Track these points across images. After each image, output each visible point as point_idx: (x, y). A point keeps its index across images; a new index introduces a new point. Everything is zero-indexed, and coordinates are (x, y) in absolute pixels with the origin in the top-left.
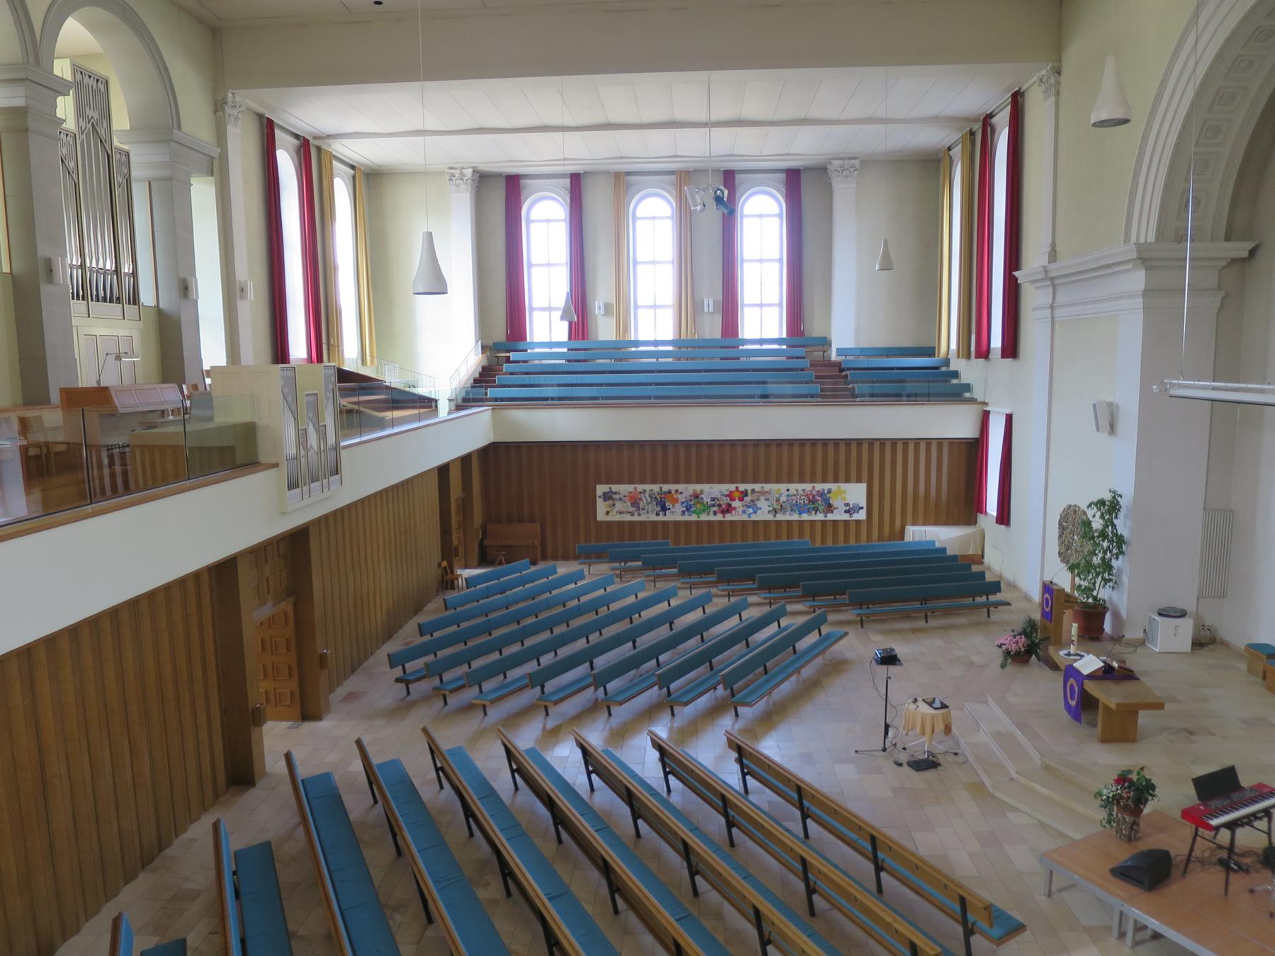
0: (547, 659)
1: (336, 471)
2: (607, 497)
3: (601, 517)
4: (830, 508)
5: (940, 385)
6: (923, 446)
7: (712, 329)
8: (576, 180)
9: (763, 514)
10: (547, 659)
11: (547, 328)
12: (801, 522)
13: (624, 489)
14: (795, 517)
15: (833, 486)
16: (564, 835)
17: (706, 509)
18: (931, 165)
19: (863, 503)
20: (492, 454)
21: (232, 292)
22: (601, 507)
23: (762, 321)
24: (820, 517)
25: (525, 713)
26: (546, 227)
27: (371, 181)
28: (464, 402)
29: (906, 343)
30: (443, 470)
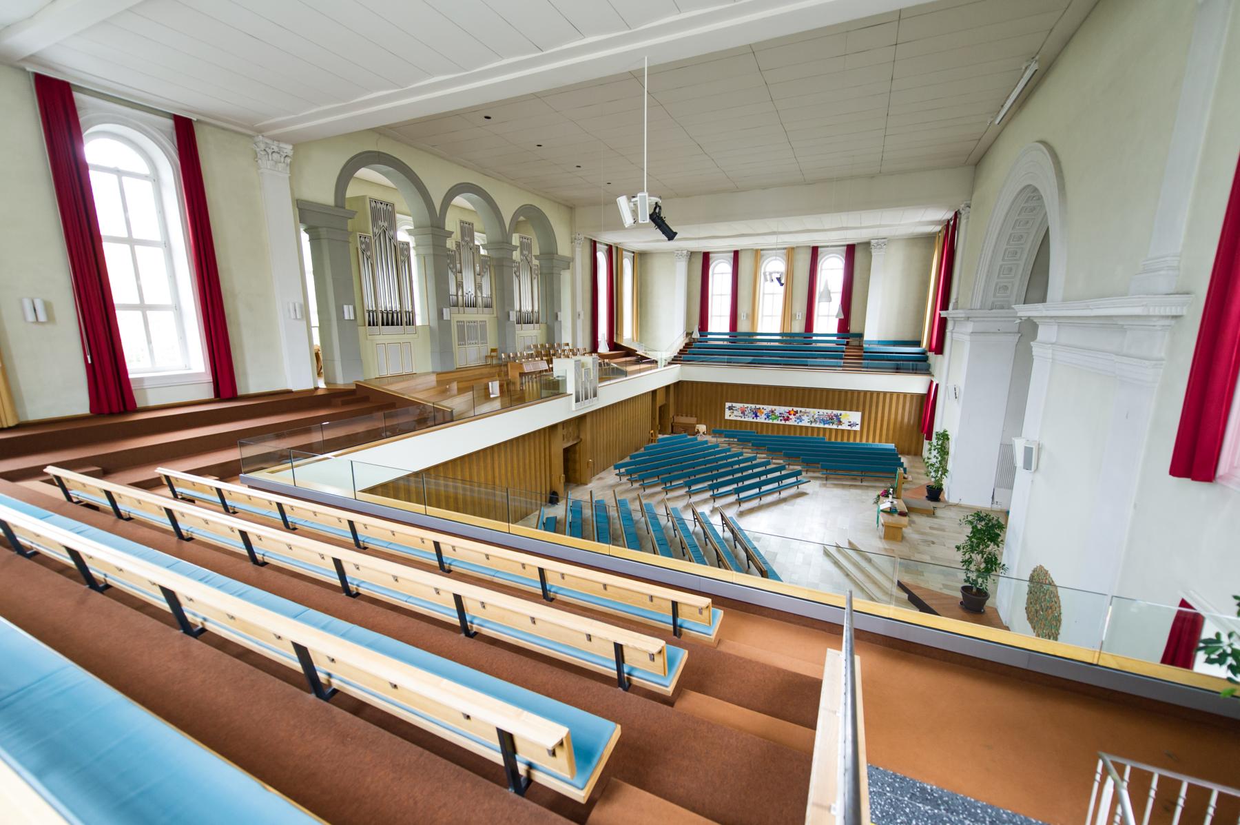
0: (763, 478)
1: (595, 395)
2: (730, 408)
3: (727, 417)
4: (840, 422)
5: (919, 365)
6: (895, 397)
7: (798, 327)
8: (736, 253)
9: (805, 423)
10: (763, 478)
11: (719, 323)
12: (825, 429)
13: (738, 405)
14: (822, 426)
15: (843, 412)
16: (262, 476)
17: (777, 418)
18: (929, 238)
19: (859, 422)
20: (679, 385)
21: (575, 315)
22: (727, 413)
23: (826, 322)
24: (835, 427)
25: (705, 501)
26: (721, 275)
27: (641, 257)
28: (674, 361)
29: (892, 338)
30: (654, 392)
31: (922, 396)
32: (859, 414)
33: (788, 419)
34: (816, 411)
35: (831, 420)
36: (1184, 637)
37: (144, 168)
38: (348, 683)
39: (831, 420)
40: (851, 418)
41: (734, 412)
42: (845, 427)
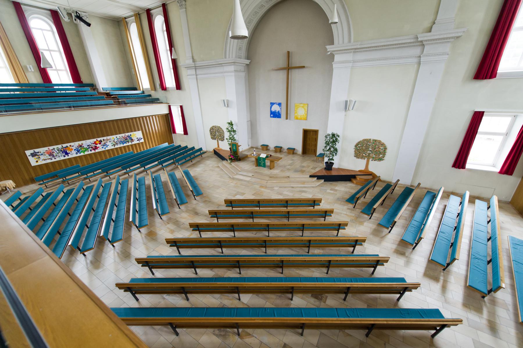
4: (132, 140)
9: (110, 147)
12: (124, 147)
13: (42, 150)
14: (122, 145)
15: (131, 133)
17: (86, 150)
24: (130, 144)
31: (168, 114)
32: (140, 132)
33: (96, 148)
34: (114, 137)
35: (126, 140)
36: (302, 334)
37: (49, 28)
38: (332, 255)
39: (126, 140)
40: (137, 135)
41: (39, 158)
42: (136, 142)
